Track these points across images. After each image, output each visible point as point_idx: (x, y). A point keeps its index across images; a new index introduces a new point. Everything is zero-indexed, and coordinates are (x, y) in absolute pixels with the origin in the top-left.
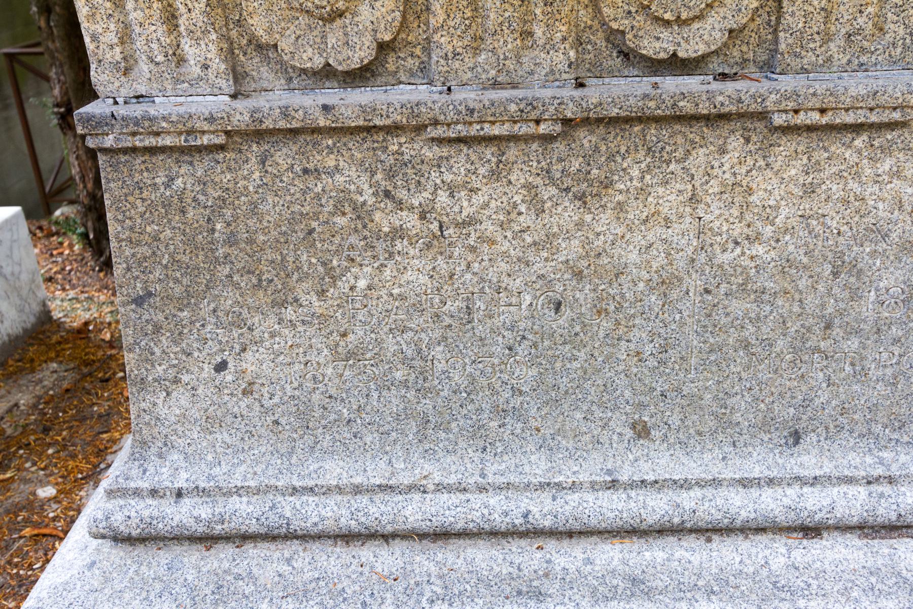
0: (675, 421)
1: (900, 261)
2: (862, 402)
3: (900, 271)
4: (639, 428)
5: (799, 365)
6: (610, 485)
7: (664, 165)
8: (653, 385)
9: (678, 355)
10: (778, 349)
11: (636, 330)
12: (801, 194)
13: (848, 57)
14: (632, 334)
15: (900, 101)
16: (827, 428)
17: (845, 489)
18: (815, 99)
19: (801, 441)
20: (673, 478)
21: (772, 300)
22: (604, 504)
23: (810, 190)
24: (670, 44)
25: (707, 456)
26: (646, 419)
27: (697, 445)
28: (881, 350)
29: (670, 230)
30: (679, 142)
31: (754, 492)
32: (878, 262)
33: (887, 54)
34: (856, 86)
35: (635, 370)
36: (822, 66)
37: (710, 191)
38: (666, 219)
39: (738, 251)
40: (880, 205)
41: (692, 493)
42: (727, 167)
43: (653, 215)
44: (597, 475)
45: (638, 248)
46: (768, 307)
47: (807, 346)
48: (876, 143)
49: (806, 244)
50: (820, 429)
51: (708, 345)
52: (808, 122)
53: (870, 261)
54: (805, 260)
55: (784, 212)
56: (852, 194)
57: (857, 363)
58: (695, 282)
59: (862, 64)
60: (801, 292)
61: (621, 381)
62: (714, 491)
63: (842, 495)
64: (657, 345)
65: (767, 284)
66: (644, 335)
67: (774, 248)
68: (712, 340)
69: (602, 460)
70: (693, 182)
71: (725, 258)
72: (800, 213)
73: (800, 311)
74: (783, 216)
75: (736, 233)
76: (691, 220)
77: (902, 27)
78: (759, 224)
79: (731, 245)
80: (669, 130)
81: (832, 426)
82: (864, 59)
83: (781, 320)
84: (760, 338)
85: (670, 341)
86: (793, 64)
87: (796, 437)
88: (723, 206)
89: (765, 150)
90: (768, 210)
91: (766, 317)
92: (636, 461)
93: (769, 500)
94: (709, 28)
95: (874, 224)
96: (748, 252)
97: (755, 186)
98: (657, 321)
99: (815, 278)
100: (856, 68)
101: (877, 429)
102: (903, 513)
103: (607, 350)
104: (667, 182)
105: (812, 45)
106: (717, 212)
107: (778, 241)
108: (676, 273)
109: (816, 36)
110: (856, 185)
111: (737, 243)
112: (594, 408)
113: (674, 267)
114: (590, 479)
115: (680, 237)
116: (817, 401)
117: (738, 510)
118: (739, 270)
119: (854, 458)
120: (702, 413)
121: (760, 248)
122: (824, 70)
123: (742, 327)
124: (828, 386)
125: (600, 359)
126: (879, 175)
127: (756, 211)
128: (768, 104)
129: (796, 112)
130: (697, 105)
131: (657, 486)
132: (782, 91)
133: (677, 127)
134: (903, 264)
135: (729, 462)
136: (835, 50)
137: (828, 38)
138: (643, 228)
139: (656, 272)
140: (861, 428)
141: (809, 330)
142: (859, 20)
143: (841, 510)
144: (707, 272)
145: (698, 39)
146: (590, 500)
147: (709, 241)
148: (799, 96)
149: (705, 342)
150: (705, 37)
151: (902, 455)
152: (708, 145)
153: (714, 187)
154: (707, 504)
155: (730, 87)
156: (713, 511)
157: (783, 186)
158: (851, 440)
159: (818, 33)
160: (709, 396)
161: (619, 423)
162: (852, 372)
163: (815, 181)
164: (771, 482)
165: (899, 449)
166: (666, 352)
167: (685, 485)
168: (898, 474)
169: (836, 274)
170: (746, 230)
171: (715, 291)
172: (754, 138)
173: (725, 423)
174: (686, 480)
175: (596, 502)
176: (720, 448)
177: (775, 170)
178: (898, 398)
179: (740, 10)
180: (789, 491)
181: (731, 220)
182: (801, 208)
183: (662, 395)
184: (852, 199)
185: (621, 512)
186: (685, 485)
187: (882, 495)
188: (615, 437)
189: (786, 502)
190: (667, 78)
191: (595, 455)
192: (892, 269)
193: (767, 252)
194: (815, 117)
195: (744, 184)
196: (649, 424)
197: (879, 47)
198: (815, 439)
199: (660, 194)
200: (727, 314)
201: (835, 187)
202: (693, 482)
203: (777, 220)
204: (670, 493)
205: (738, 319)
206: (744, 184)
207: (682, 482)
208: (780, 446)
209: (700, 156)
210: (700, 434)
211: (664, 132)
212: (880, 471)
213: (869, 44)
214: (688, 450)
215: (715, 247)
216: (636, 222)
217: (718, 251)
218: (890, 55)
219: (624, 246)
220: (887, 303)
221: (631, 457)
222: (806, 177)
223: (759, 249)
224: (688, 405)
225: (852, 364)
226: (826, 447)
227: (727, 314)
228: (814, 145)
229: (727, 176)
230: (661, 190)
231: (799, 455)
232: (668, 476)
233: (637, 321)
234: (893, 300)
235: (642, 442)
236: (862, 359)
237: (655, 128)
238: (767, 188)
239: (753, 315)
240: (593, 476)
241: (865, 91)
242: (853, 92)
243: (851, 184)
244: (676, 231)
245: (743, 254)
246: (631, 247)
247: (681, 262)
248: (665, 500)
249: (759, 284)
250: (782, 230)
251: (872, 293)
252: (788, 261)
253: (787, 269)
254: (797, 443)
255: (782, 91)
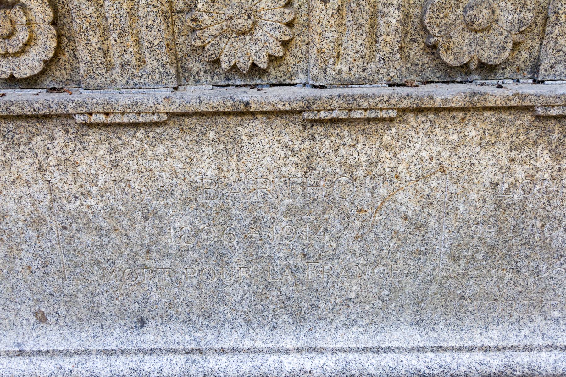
0: (62, 311)
1: (185, 211)
2: (182, 300)
3: (186, 217)
4: (39, 315)
5: (135, 276)
6: (19, 353)
7: (16, 147)
8: (44, 287)
9: (55, 269)
10: (119, 266)
11: (23, 252)
12: (110, 166)
13: (126, 79)
14: (22, 255)
15: (154, 108)
16: (161, 317)
17: (172, 357)
18: (98, 107)
19: (145, 325)
20: (59, 349)
21: (107, 234)
22: (13, 366)
23: (115, 165)
24: (8, 69)
25: (84, 334)
26: (43, 310)
27: (78, 327)
28: (186, 267)
29: (31, 188)
30: (22, 132)
31: (113, 358)
32: (171, 211)
33: (150, 77)
34: (124, 98)
35: (30, 278)
36: (110, 84)
37: (51, 164)
38: (27, 181)
39: (78, 202)
40: (163, 174)
41: (72, 359)
42: (57, 149)
43: (17, 179)
44: (10, 347)
45: (13, 199)
46: (106, 239)
47: (138, 264)
48: (150, 135)
49: (121, 199)
50: (157, 318)
51: (73, 263)
52: (98, 121)
53: (165, 210)
54: (123, 209)
55: (102, 179)
56: (143, 167)
57: (173, 275)
58: (55, 222)
59: (136, 84)
60: (125, 230)
61: (22, 285)
62: (87, 358)
63: (169, 361)
64: (40, 262)
65: (102, 224)
66: (30, 256)
67: (102, 201)
68: (75, 259)
69: (15, 337)
70: (38, 158)
71: (72, 206)
72: (113, 179)
73: (128, 241)
74: (102, 180)
75: (74, 191)
76: (43, 182)
77: (155, 61)
78: (88, 185)
79: (73, 199)
80: (14, 124)
81: (164, 315)
82: (136, 80)
83: (117, 247)
84: (106, 258)
85: (48, 260)
86: (91, 83)
87: (142, 322)
88: (61, 173)
89: (80, 138)
90: (91, 176)
91: (106, 245)
92: (37, 337)
93: (121, 364)
94: (31, 59)
95: (163, 187)
96: (85, 203)
97: (79, 161)
98: (36, 246)
99: (133, 221)
100: (133, 86)
101: (194, 318)
102: (207, 374)
103: (8, 265)
104: (21, 158)
105: (100, 71)
106: (59, 177)
107: (102, 196)
108: (42, 216)
109: (100, 65)
110: (145, 161)
111: (76, 198)
112: (8, 302)
113: (40, 212)
114: (5, 350)
115: (38, 193)
116: (152, 300)
117: (99, 371)
118: (82, 215)
119: (178, 337)
120: (79, 307)
121: (92, 201)
122: (113, 87)
123: (93, 251)
124: (157, 290)
125: (5, 271)
126: (157, 155)
127: (84, 177)
128: (69, 109)
129: (91, 114)
130: (23, 109)
131: (49, 354)
132: (76, 101)
133: (19, 122)
134: (187, 212)
135: (97, 339)
136: (116, 75)
137: (109, 67)
138: (13, 187)
139: (28, 215)
140: (183, 317)
141: (136, 253)
142: (126, 56)
143: (166, 372)
144: (61, 216)
145: (25, 66)
146: (5, 363)
147: (58, 196)
148: (88, 104)
149: (71, 261)
150: (29, 65)
151: (210, 335)
152: (42, 134)
153: (52, 161)
154: (80, 367)
155: (55, 97)
156: (83, 371)
157: (97, 161)
158: (178, 325)
159: (102, 64)
160: (81, 295)
161: (26, 312)
162: (170, 280)
163: (117, 158)
164: (123, 352)
165: (208, 331)
166: (47, 267)
167: (67, 353)
168: (204, 347)
169: (145, 218)
170: (80, 189)
171: (69, 228)
172: (71, 131)
173: (95, 313)
174: (67, 351)
175: (9, 365)
176: (93, 329)
177: (90, 151)
178: (204, 298)
179: (46, 48)
180: (135, 358)
181: (69, 182)
182: (113, 175)
183: (51, 294)
184: (144, 170)
185: (23, 371)
186: (67, 353)
187: (194, 362)
188: (25, 322)
189: (132, 365)
190: (17, 90)
191: (11, 333)
192: (181, 215)
193: (98, 203)
194: (102, 118)
195: (72, 160)
196: (45, 313)
197: (144, 73)
198: (154, 324)
199: (18, 165)
200: (81, 243)
201: (131, 163)
202: (73, 352)
203: (98, 183)
204: (58, 359)
205: (88, 246)
206: (72, 160)
207: (66, 352)
208: (132, 328)
209: (39, 142)
210: (80, 320)
211: (11, 126)
212: (193, 346)
213: (137, 71)
214: (72, 330)
215: (63, 199)
216: (8, 183)
217: (65, 202)
218: (153, 79)
219: (3, 198)
220: (183, 237)
221: (34, 335)
222: (111, 156)
223: (91, 202)
224: (69, 301)
225: (170, 276)
226: (161, 329)
227: (81, 243)
228: (111, 135)
229: (59, 154)
230: (18, 163)
231: (143, 334)
232: (55, 348)
233: (23, 247)
234: (186, 235)
235: (42, 325)
236: (175, 273)
237: (5, 123)
238: (87, 163)
239: (98, 244)
240: (7, 348)
241: (129, 102)
242: (121, 102)
243: (141, 161)
244: (35, 189)
245: (82, 204)
246: (8, 199)
247: (43, 209)
248: (53, 364)
249: (97, 224)
250: (104, 189)
251: (172, 230)
252: (112, 209)
253: (113, 215)
254: (142, 326)
255: (76, 101)
